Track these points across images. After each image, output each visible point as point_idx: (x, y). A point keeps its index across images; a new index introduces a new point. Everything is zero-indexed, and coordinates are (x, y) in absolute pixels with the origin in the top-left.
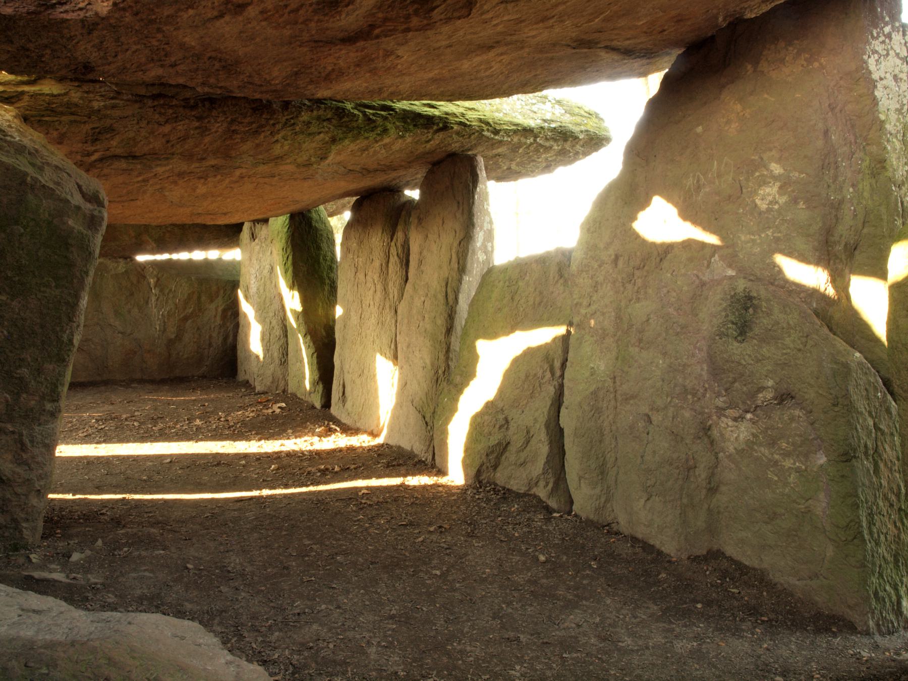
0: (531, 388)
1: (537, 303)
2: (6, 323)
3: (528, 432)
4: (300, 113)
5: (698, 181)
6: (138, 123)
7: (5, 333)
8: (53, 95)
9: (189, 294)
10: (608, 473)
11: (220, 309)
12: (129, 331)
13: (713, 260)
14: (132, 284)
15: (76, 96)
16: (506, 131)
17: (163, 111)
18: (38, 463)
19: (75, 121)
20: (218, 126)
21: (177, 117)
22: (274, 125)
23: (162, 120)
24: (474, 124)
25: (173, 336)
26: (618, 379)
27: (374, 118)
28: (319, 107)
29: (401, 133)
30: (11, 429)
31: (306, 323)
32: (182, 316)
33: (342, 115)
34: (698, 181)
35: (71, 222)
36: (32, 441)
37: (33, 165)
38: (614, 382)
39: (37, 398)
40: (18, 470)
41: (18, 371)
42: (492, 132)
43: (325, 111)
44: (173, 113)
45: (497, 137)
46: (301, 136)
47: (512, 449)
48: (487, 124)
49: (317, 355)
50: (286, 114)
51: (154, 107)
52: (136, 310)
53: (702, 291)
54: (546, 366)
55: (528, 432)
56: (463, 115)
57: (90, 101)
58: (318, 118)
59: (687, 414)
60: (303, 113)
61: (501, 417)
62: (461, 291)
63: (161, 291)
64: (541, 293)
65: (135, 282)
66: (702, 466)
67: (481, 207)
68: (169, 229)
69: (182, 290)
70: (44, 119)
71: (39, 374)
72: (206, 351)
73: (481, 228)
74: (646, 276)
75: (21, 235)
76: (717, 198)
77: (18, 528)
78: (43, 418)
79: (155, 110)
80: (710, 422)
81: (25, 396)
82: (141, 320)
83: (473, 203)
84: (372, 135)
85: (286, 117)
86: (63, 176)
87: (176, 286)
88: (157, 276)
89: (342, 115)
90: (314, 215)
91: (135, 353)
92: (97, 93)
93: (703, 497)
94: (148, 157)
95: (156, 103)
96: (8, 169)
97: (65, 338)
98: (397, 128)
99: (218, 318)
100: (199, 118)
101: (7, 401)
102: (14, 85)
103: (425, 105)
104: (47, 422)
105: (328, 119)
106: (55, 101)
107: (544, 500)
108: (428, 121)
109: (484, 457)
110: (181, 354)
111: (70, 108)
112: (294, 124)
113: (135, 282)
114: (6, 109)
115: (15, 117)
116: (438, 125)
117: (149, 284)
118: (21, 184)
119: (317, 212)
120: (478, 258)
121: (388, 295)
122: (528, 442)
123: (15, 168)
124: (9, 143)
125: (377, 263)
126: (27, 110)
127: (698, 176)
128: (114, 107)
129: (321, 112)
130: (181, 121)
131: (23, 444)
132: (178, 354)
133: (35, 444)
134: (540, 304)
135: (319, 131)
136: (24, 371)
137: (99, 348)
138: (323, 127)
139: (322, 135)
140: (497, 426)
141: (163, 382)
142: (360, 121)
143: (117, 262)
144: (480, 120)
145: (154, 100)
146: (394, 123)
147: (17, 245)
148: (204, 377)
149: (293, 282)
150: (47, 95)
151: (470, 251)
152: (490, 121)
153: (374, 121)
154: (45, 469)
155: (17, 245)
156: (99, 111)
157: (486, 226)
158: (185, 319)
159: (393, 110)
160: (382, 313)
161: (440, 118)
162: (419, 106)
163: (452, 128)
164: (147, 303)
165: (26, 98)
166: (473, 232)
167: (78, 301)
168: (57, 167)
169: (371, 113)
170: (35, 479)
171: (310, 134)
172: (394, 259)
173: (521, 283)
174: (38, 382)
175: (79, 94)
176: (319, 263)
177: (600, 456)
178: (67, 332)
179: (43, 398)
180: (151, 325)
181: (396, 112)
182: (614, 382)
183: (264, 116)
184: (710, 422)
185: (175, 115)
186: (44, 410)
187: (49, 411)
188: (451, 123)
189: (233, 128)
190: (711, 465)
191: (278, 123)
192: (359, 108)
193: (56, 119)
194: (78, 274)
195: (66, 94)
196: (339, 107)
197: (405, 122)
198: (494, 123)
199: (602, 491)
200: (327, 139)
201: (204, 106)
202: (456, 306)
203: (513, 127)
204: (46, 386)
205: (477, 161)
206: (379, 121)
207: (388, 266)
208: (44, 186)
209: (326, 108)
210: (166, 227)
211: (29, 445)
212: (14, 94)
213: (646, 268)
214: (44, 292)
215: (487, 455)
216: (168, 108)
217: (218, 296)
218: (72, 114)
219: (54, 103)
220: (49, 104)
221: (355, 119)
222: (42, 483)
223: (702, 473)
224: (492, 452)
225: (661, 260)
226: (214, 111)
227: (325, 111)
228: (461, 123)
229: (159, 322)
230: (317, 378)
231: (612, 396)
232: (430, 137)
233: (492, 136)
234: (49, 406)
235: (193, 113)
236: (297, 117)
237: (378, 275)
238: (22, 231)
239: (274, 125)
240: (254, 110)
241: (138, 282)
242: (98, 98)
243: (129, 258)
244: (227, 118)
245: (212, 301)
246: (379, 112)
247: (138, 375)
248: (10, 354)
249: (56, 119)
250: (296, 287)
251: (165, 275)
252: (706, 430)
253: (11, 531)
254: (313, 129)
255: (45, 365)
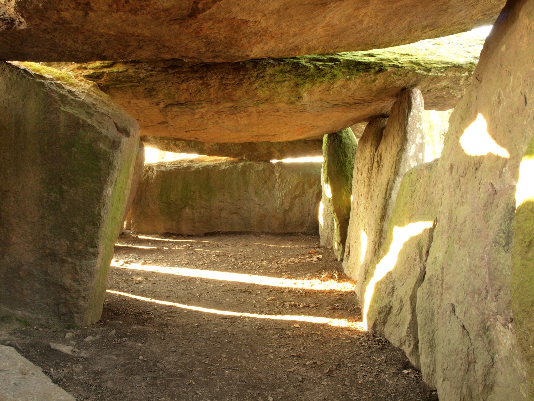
0: (409, 267)
1: (424, 200)
2: (67, 202)
3: (401, 302)
4: (265, 69)
5: (499, 97)
6: (166, 84)
7: (67, 207)
8: (118, 72)
9: (297, 183)
10: (435, 347)
11: (315, 193)
12: (262, 204)
13: (504, 170)
14: (266, 176)
15: (131, 72)
16: (436, 68)
17: (178, 76)
18: (84, 281)
19: (133, 86)
20: (214, 81)
21: (188, 79)
22: (249, 78)
23: (179, 80)
24: (405, 65)
25: (287, 208)
26: (445, 269)
27: (323, 68)
28: (280, 64)
29: (347, 77)
30: (70, 261)
31: (333, 205)
32: (293, 196)
33: (297, 67)
34: (499, 97)
35: (101, 145)
36: (81, 269)
37: (88, 113)
38: (442, 272)
39: (83, 245)
40: (73, 284)
41: (72, 229)
42: (425, 71)
43: (284, 66)
44: (185, 76)
45: (430, 74)
46: (272, 85)
47: (395, 310)
48: (419, 64)
49: (340, 226)
50: (255, 70)
51: (173, 73)
52: (267, 191)
53: (493, 199)
54: (417, 251)
55: (401, 302)
56: (396, 60)
57: (139, 73)
58: (281, 71)
59: (474, 311)
60: (267, 69)
61: (391, 286)
62: (394, 188)
63: (282, 181)
64: (427, 193)
65: (268, 175)
66: (480, 362)
67: (414, 126)
68: (285, 144)
69: (294, 180)
70: (116, 86)
71: (83, 231)
72: (306, 218)
73: (414, 142)
74: (467, 183)
75: (75, 153)
76: (510, 111)
77: (72, 317)
78: (87, 257)
79: (174, 76)
80: (489, 324)
81: (76, 243)
82: (269, 197)
83: (407, 124)
84: (325, 80)
85: (256, 73)
86: (106, 118)
87: (290, 178)
88: (280, 172)
89: (297, 67)
90: (344, 135)
91: (266, 216)
92: (143, 68)
93: (480, 392)
94: (188, 103)
95: (174, 71)
96: (70, 116)
97: (96, 212)
98: (343, 73)
99: (314, 198)
100: (201, 78)
101: (68, 245)
102: (99, 69)
103: (365, 55)
104: (91, 259)
105: (289, 71)
106: (120, 75)
107: (408, 356)
108: (366, 67)
109: (377, 315)
110: (292, 219)
111: (128, 79)
112: (263, 76)
113: (268, 175)
114: (89, 82)
115: (93, 87)
116: (375, 69)
117: (276, 176)
118: (76, 124)
119: (346, 132)
120: (410, 165)
121: (371, 189)
122: (401, 309)
123: (73, 115)
124: (76, 102)
125: (367, 167)
126: (107, 82)
127: (500, 91)
128: (151, 76)
129: (281, 67)
130: (190, 80)
131: (76, 270)
132: (290, 219)
133: (82, 270)
134: (426, 201)
135: (284, 79)
136: (75, 229)
137: (246, 212)
138: (286, 77)
139: (286, 82)
140: (387, 293)
141: (280, 234)
142: (311, 71)
143: (259, 163)
144: (412, 62)
145: (172, 69)
146: (340, 70)
147: (73, 159)
148: (304, 233)
149: (327, 178)
150: (116, 72)
151: (403, 159)
152: (421, 62)
153: (322, 70)
154: (88, 285)
155: (73, 159)
156: (144, 79)
157: (418, 141)
158: (295, 198)
159: (338, 61)
160: (367, 201)
161: (376, 63)
162: (359, 55)
163: (386, 70)
164: (274, 188)
165: (106, 75)
166: (406, 145)
167: (103, 191)
168: (103, 113)
169: (320, 65)
170: (82, 290)
171: (278, 82)
172: (375, 164)
173: (417, 185)
174: (83, 236)
175: (133, 70)
176: (345, 166)
177: (431, 332)
178: (97, 208)
179: (86, 245)
180: (275, 201)
181: (340, 62)
182: (442, 272)
183: (241, 73)
184: (489, 324)
185: (186, 78)
186: (88, 252)
187: (91, 252)
188: (385, 66)
189: (224, 82)
190: (487, 363)
191: (252, 77)
192: (312, 62)
193: (122, 85)
194: (103, 175)
195: (126, 71)
196: (295, 63)
197: (349, 69)
198: (425, 63)
199: (431, 361)
200: (292, 85)
201: (203, 70)
202: (389, 199)
203: (445, 65)
204: (88, 239)
205: (412, 93)
206: (327, 69)
207: (372, 169)
208: (89, 125)
209: (285, 64)
210: (283, 143)
211: (79, 270)
212: (100, 74)
213: (467, 176)
214: (85, 185)
215: (379, 313)
216: (182, 74)
217: (315, 185)
218: (131, 82)
219: (120, 77)
220: (117, 77)
221: (308, 70)
222: (86, 293)
223: (479, 369)
224: (382, 312)
225: (476, 169)
226: (209, 72)
227: (284, 66)
228: (394, 66)
229: (279, 199)
230: (339, 241)
231: (440, 283)
232: (373, 78)
233: (426, 73)
234: (91, 250)
235: (197, 75)
236: (264, 71)
237: (366, 175)
238: (76, 150)
239: (249, 78)
240: (235, 70)
241: (270, 175)
242: (143, 71)
243: (268, 161)
244: (218, 76)
245: (311, 188)
246: (327, 63)
247: (266, 230)
248: (69, 219)
249: (122, 85)
250: (329, 182)
251: (285, 172)
252: (485, 329)
253: (69, 317)
254: (278, 79)
255: (86, 227)
